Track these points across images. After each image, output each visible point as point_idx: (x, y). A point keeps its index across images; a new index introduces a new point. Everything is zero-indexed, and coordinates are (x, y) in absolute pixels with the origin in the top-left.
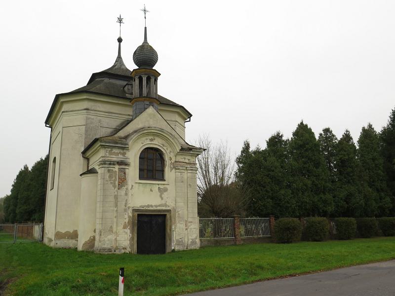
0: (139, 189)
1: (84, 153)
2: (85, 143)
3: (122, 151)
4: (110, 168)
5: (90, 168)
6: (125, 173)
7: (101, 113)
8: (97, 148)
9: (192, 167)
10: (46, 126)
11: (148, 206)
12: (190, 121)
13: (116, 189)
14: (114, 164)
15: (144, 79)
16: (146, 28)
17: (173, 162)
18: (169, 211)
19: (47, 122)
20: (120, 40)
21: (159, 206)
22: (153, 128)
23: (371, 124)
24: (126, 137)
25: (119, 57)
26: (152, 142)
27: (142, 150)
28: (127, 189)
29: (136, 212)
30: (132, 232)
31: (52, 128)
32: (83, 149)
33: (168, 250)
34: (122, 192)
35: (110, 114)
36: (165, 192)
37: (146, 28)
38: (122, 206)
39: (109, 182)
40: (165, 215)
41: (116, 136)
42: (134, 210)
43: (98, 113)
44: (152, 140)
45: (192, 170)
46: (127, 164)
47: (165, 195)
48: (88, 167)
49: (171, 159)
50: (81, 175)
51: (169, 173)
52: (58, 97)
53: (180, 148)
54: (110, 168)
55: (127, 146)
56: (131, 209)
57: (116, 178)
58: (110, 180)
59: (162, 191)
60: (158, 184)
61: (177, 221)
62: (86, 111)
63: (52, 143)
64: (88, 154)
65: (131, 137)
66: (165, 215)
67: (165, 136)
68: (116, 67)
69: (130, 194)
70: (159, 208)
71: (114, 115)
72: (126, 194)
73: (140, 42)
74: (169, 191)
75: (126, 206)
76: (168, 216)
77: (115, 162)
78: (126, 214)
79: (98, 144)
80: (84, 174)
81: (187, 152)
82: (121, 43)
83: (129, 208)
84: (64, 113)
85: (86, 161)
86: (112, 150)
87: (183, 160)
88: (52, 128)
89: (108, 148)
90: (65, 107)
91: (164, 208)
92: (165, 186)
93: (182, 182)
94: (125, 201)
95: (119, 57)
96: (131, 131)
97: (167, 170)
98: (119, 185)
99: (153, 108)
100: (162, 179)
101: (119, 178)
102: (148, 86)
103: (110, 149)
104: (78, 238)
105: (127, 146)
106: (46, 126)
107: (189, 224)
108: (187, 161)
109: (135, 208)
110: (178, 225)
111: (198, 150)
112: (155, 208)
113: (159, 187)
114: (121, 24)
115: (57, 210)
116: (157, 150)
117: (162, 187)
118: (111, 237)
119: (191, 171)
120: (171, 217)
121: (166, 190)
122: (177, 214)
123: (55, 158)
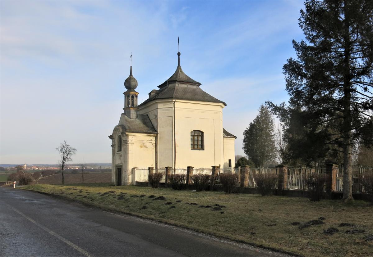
16: (131, 67)
25: (179, 65)
37: (131, 67)
73: (128, 76)
82: (180, 56)
95: (179, 65)
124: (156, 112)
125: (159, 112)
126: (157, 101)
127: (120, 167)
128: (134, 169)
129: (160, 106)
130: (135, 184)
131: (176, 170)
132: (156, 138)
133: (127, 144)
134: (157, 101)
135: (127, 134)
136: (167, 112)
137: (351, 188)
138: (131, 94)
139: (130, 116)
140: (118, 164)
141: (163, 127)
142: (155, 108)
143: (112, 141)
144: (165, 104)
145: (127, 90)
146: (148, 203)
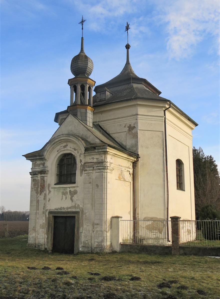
0: (54, 193)
3: (42, 162)
4: (35, 178)
6: (44, 181)
9: (98, 166)
11: (61, 209)
14: (36, 174)
16: (82, 38)
17: (83, 164)
18: (77, 213)
20: (128, 47)
21: (70, 208)
22: (61, 136)
25: (128, 63)
26: (65, 149)
27: (57, 157)
28: (45, 194)
29: (51, 214)
30: (48, 234)
33: (76, 251)
34: (41, 197)
36: (75, 194)
37: (82, 38)
39: (34, 190)
40: (74, 217)
42: (50, 212)
44: (65, 147)
45: (99, 169)
47: (75, 198)
49: (81, 161)
51: (79, 178)
53: (84, 149)
54: (35, 178)
55: (43, 157)
56: (48, 211)
58: (34, 188)
59: (73, 193)
60: (69, 188)
61: (84, 224)
66: (74, 217)
70: (69, 210)
72: (45, 199)
73: (77, 52)
74: (78, 193)
75: (44, 209)
76: (76, 218)
77: (37, 172)
78: (44, 216)
81: (92, 151)
82: (129, 50)
83: (47, 210)
86: (36, 162)
87: (92, 161)
91: (74, 210)
92: (75, 188)
94: (43, 204)
95: (128, 63)
97: (78, 172)
98: (40, 191)
101: (41, 186)
104: (28, 234)
105: (43, 157)
107: (95, 226)
108: (95, 160)
109: (51, 211)
110: (85, 226)
111: (102, 147)
112: (67, 210)
113: (70, 190)
114: (129, 30)
116: (70, 154)
117: (72, 190)
118: (85, 224)
119: (99, 171)
120: (79, 218)
121: (75, 192)
122: (84, 215)
124: (135, 121)
125: (140, 122)
126: (139, 103)
127: (73, 215)
128: (114, 219)
129: (141, 111)
130: (117, 249)
131: (141, 221)
132: (135, 164)
133: (104, 169)
134: (139, 103)
135: (108, 150)
136: (153, 122)
137: (49, 231)
138: (88, 82)
139: (86, 120)
140: (55, 209)
141: (147, 148)
142: (135, 113)
143: (33, 164)
144: (150, 109)
145: (75, 76)
146: (17, 268)
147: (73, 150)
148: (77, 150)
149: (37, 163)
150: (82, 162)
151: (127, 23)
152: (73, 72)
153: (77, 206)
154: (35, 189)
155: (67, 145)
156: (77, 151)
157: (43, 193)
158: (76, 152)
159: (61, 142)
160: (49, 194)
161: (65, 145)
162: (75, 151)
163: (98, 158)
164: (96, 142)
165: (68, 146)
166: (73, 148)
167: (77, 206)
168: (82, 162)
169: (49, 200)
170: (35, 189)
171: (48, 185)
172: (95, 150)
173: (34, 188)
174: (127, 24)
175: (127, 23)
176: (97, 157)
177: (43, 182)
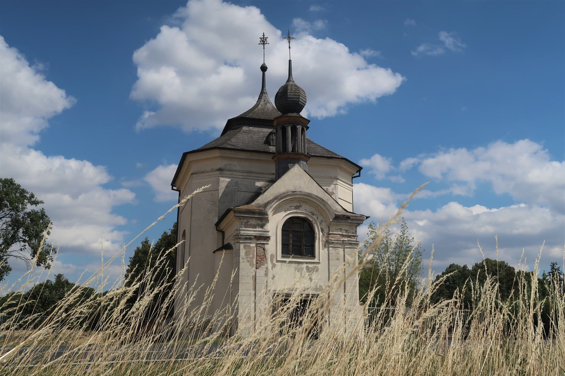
1: (217, 224)
2: (219, 212)
5: (225, 243)
6: (264, 249)
7: (238, 174)
8: (231, 219)
10: (173, 189)
12: (359, 176)
13: (254, 268)
15: (289, 129)
16: (290, 61)
19: (173, 184)
23: (148, 239)
24: (266, 205)
28: (267, 268)
31: (180, 191)
32: (216, 220)
34: (261, 272)
35: (249, 174)
37: (290, 61)
38: (261, 291)
41: (253, 203)
43: (235, 173)
46: (267, 238)
48: (223, 242)
50: (214, 252)
52: (185, 155)
57: (253, 255)
58: (247, 258)
60: (307, 263)
62: (218, 172)
63: (180, 212)
64: (222, 226)
65: (271, 205)
67: (313, 201)
68: (260, 106)
69: (270, 275)
71: (254, 175)
72: (266, 275)
79: (231, 215)
80: (217, 250)
82: (266, 73)
84: (194, 176)
85: (220, 235)
88: (180, 191)
89: (244, 219)
90: (194, 168)
93: (338, 259)
96: (272, 198)
98: (257, 263)
99: (299, 168)
100: (313, 255)
102: (293, 139)
103: (245, 221)
106: (173, 189)
113: (307, 266)
114: (266, 45)
115: (192, 206)
123: (184, 231)
147: (310, 214)
148: (316, 215)
149: (250, 223)
150: (323, 232)
151: (264, 34)
152: (277, 102)
153: (318, 287)
154: (248, 260)
155: (301, 206)
156: (316, 216)
157: (262, 266)
158: (314, 217)
159: (293, 201)
160: (273, 269)
161: (297, 206)
162: (314, 215)
163: (348, 230)
164: (337, 209)
165: (301, 207)
166: (310, 211)
167: (318, 287)
168: (323, 232)
169: (273, 277)
170: (248, 259)
171: (271, 256)
172: (348, 220)
173: (247, 258)
174: (264, 36)
175: (264, 34)
176: (347, 229)
177: (263, 251)
